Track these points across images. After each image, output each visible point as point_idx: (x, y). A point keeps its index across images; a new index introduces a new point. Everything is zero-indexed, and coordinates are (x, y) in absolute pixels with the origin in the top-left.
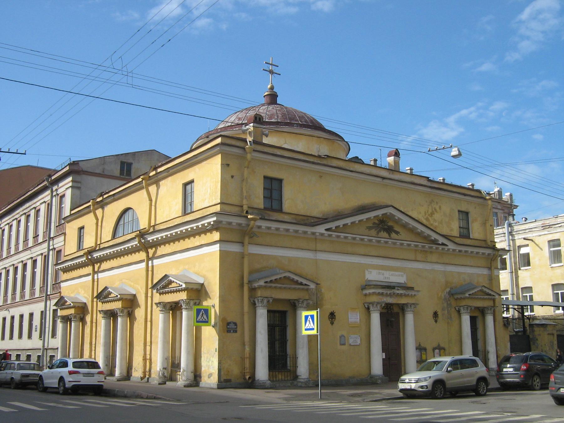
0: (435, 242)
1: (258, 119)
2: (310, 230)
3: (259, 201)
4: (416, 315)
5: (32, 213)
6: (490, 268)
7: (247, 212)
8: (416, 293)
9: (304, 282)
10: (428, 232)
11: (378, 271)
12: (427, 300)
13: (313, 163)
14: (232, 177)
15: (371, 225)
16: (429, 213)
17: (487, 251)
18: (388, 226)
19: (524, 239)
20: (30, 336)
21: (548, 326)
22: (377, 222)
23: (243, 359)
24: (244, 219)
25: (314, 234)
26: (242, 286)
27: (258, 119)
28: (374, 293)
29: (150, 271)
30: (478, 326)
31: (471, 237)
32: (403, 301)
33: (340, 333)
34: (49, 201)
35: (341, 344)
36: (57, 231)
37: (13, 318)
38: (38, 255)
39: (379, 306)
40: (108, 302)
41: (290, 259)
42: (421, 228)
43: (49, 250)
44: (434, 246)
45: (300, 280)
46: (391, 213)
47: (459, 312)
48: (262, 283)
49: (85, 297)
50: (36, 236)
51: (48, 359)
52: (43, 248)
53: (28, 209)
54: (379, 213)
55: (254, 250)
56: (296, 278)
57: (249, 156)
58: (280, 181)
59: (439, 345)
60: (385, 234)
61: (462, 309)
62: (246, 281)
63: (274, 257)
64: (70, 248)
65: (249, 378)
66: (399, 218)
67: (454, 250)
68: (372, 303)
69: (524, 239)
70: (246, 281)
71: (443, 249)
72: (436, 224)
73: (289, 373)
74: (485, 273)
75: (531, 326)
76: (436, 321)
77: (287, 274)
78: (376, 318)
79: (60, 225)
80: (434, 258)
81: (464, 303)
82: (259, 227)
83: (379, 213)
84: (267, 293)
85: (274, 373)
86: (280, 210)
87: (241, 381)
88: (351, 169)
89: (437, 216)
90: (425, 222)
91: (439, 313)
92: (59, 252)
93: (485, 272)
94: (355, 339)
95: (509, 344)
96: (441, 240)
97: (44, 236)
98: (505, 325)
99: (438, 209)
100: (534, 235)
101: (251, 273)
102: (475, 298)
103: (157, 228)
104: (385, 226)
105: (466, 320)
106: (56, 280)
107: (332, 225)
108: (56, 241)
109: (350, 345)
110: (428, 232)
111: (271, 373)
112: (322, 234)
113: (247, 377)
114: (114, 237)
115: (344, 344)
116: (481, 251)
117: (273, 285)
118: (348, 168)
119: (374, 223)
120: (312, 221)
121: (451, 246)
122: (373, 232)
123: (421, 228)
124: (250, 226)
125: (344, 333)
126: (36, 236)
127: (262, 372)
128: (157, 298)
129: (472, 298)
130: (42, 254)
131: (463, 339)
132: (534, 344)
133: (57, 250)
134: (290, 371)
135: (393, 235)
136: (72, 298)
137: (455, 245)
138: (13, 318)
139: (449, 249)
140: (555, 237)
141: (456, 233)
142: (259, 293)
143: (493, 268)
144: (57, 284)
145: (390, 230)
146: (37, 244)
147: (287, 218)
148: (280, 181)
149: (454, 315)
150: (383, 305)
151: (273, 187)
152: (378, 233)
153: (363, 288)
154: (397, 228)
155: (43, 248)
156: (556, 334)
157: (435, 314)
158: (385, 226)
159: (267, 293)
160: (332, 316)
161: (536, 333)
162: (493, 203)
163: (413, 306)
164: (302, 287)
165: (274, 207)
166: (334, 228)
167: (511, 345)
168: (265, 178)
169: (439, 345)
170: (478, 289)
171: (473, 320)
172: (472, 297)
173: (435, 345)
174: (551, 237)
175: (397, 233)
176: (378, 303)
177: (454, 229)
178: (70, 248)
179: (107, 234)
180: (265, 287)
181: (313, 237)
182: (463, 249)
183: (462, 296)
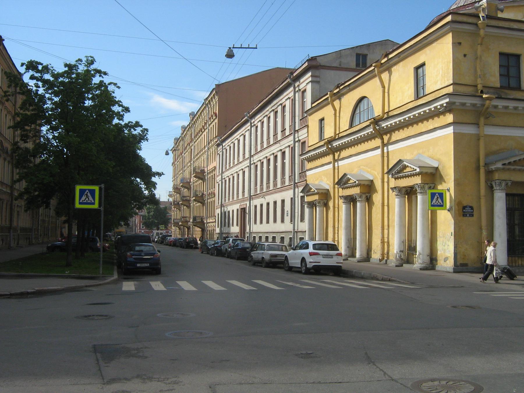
3: (495, 80)
5: (279, 109)
7: (482, 92)
14: (465, 55)
24: (478, 99)
26: (478, 168)
36: (301, 124)
37: (268, 204)
38: (286, 147)
49: (327, 183)
50: (283, 130)
52: (290, 141)
53: (276, 106)
57: (482, 32)
62: (482, 163)
64: (313, 139)
70: (482, 163)
79: (303, 119)
82: (496, 107)
84: (506, 176)
92: (304, 143)
97: (290, 130)
101: (487, 155)
103: (391, 114)
108: (300, 133)
111: (510, 258)
114: (351, 126)
117: (512, 167)
124: (486, 106)
126: (283, 130)
128: (393, 183)
130: (289, 146)
136: (316, 185)
138: (268, 204)
142: (496, 176)
144: (303, 173)
146: (285, 137)
155: (290, 141)
159: (506, 176)
178: (313, 139)
179: (344, 124)
180: (503, 169)
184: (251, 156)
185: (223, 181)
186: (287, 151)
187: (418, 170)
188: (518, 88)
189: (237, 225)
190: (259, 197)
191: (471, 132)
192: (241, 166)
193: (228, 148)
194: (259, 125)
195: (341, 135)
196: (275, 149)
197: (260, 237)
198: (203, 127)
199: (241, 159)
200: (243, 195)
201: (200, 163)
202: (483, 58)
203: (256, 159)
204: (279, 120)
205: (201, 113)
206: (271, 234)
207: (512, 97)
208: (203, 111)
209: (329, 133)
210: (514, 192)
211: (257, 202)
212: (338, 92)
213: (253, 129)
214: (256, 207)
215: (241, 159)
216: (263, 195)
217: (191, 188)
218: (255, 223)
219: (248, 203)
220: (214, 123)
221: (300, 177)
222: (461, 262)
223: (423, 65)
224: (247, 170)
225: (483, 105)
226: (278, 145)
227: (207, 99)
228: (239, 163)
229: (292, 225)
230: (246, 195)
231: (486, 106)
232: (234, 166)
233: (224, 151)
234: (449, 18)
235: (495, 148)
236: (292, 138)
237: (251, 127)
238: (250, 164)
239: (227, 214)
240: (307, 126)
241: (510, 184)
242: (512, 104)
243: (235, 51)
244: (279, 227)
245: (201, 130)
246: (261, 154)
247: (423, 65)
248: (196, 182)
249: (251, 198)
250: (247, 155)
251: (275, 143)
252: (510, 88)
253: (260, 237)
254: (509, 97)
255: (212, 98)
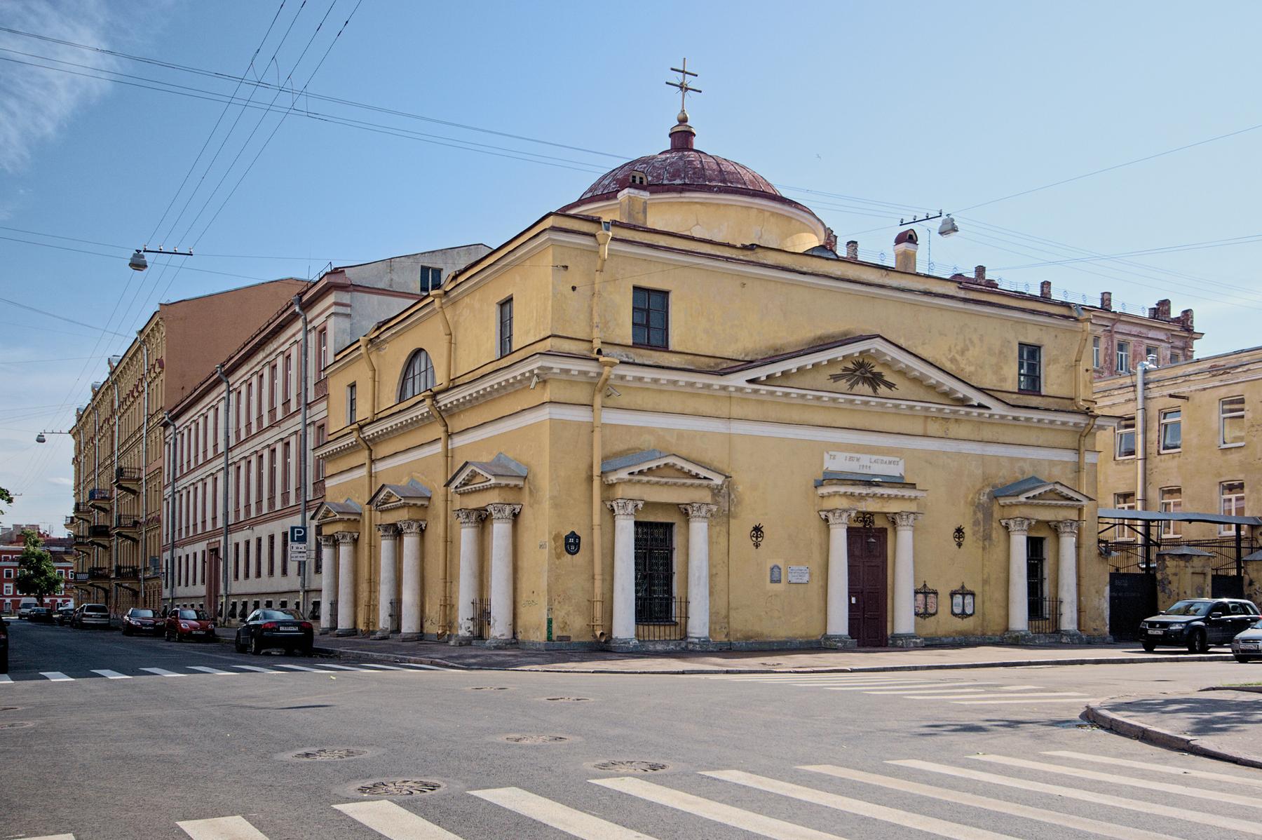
0: (964, 402)
1: (638, 181)
2: (716, 382)
3: (625, 333)
4: (915, 529)
5: (280, 362)
6: (1077, 450)
7: (599, 352)
8: (919, 494)
9: (703, 473)
10: (949, 383)
11: (848, 455)
12: (945, 505)
13: (727, 259)
14: (574, 288)
15: (839, 372)
16: (959, 348)
17: (1072, 419)
18: (874, 374)
19: (1171, 396)
20: (284, 572)
21: (1195, 559)
22: (851, 366)
23: (591, 602)
24: (594, 364)
25: (724, 388)
26: (590, 479)
27: (638, 181)
28: (836, 494)
29: (448, 454)
30: (1045, 555)
31: (1043, 393)
32: (892, 507)
33: (770, 564)
34: (302, 342)
35: (772, 581)
36: (317, 393)
37: (259, 540)
38: (290, 435)
39: (845, 516)
40: (388, 510)
41: (680, 435)
42: (935, 376)
43: (306, 426)
44: (963, 410)
45: (695, 470)
46: (877, 350)
47: (1007, 527)
48: (623, 475)
49: (360, 500)
50: (286, 403)
51: (311, 607)
52: (296, 423)
53: (273, 356)
54: (854, 349)
55: (611, 417)
56: (688, 466)
57: (605, 251)
58: (665, 294)
59: (963, 587)
60: (866, 389)
61: (1012, 523)
62: (597, 471)
63: (651, 431)
64: (339, 422)
65: (602, 634)
66: (893, 358)
67: (1002, 417)
68: (833, 511)
69: (1171, 396)
70: (597, 471)
71: (979, 415)
72: (972, 369)
73: (673, 629)
74: (1066, 459)
75: (1160, 557)
76: (959, 545)
77: (671, 460)
78: (839, 538)
79: (321, 384)
80: (963, 430)
81: (1017, 512)
82: (622, 377)
83: (854, 349)
84: (634, 492)
85: (657, 629)
86: (664, 347)
87: (588, 639)
88: (805, 269)
89: (973, 353)
90: (948, 366)
91: (968, 531)
92: (322, 427)
93: (1069, 456)
94: (798, 572)
95: (1107, 589)
96: (977, 398)
97: (299, 403)
98: (1101, 554)
99: (975, 338)
100: (1193, 388)
101: (605, 459)
102: (1037, 505)
103: (458, 382)
104: (864, 373)
105: (1019, 543)
106: (318, 476)
107: (761, 373)
108: (315, 409)
109: (790, 582)
110: (949, 383)
111: (641, 627)
112: (740, 390)
113: (598, 633)
114: (401, 399)
115: (779, 581)
116: (1060, 418)
117: (645, 479)
118: (798, 268)
119: (846, 369)
120: (725, 366)
121: (997, 409)
122: (843, 384)
123: (935, 376)
124: (604, 376)
125: (780, 563)
126: (286, 403)
127: (624, 626)
128: (458, 502)
129: (1031, 505)
130: (296, 432)
131: (1011, 577)
132: (1163, 591)
133: (318, 424)
134: (676, 624)
135: (883, 390)
136: (338, 505)
137: (1006, 407)
138: (259, 540)
139: (991, 416)
140: (1236, 391)
141: (1012, 385)
142: (620, 492)
143: (1082, 450)
144: (319, 484)
145: (875, 380)
146: (288, 416)
147: (674, 360)
148: (665, 294)
149: (998, 534)
150: (853, 515)
151: (651, 310)
152: (852, 386)
153: (819, 484)
154: (888, 377)
155: (296, 423)
156: (1210, 573)
157: (959, 531)
158: (864, 373)
159: (634, 492)
160: (757, 529)
161: (1169, 571)
162: (1094, 328)
163: (912, 517)
164: (697, 482)
165: (653, 342)
166: (763, 378)
167: (1111, 591)
168: (635, 288)
169: (963, 587)
170: (1048, 488)
171: (1035, 547)
172: (1032, 502)
173: (956, 587)
174: (1223, 392)
175: (890, 386)
176: (845, 511)
177: (1010, 376)
178: (339, 422)
179: (389, 398)
180: (630, 481)
181: (723, 393)
182: (1022, 414)
183: (1014, 500)
184: (229, 449)
185: (177, 496)
186: (293, 441)
187: (493, 481)
188: (664, 347)
189: (203, 581)
190: (241, 529)
191: (581, 419)
192: (209, 469)
193: (186, 432)
194: (244, 389)
195: (380, 416)
196: (271, 437)
197: (245, 604)
198: (137, 387)
199: (210, 455)
200: (214, 523)
201: (135, 460)
202: (605, 294)
203: (236, 455)
204: (279, 381)
205: (131, 359)
206: (277, 597)
207: (686, 357)
208: (134, 354)
209: (363, 412)
210: (651, 519)
211: (239, 537)
212: (377, 337)
213: (233, 396)
214: (237, 545)
215: (210, 455)
216: (252, 523)
217: (112, 509)
218: (237, 577)
219: (222, 539)
220: (158, 381)
221: (315, 491)
222: (560, 633)
223: (509, 300)
224: (221, 476)
225: (599, 374)
226: (276, 430)
227: (141, 332)
228: (207, 462)
229: (300, 579)
230: (220, 524)
231: (604, 376)
232: (198, 467)
233: (179, 437)
234: (549, 222)
235: (620, 446)
236: (299, 418)
237: (229, 392)
238: (228, 466)
239: (183, 560)
240: (326, 396)
241: (640, 505)
242: (648, 374)
243: (148, 257)
244: (279, 583)
245: (132, 392)
246: (247, 446)
247: (509, 300)
248: (124, 497)
249: (228, 530)
250: (221, 448)
251: (272, 426)
252: (650, 346)
253: (245, 604)
254: (690, 357)
255: (152, 330)
